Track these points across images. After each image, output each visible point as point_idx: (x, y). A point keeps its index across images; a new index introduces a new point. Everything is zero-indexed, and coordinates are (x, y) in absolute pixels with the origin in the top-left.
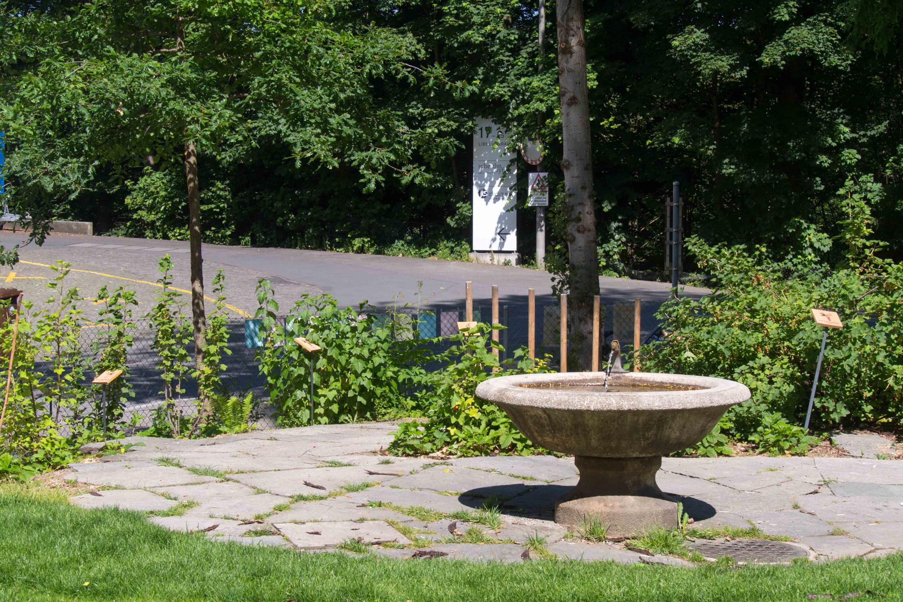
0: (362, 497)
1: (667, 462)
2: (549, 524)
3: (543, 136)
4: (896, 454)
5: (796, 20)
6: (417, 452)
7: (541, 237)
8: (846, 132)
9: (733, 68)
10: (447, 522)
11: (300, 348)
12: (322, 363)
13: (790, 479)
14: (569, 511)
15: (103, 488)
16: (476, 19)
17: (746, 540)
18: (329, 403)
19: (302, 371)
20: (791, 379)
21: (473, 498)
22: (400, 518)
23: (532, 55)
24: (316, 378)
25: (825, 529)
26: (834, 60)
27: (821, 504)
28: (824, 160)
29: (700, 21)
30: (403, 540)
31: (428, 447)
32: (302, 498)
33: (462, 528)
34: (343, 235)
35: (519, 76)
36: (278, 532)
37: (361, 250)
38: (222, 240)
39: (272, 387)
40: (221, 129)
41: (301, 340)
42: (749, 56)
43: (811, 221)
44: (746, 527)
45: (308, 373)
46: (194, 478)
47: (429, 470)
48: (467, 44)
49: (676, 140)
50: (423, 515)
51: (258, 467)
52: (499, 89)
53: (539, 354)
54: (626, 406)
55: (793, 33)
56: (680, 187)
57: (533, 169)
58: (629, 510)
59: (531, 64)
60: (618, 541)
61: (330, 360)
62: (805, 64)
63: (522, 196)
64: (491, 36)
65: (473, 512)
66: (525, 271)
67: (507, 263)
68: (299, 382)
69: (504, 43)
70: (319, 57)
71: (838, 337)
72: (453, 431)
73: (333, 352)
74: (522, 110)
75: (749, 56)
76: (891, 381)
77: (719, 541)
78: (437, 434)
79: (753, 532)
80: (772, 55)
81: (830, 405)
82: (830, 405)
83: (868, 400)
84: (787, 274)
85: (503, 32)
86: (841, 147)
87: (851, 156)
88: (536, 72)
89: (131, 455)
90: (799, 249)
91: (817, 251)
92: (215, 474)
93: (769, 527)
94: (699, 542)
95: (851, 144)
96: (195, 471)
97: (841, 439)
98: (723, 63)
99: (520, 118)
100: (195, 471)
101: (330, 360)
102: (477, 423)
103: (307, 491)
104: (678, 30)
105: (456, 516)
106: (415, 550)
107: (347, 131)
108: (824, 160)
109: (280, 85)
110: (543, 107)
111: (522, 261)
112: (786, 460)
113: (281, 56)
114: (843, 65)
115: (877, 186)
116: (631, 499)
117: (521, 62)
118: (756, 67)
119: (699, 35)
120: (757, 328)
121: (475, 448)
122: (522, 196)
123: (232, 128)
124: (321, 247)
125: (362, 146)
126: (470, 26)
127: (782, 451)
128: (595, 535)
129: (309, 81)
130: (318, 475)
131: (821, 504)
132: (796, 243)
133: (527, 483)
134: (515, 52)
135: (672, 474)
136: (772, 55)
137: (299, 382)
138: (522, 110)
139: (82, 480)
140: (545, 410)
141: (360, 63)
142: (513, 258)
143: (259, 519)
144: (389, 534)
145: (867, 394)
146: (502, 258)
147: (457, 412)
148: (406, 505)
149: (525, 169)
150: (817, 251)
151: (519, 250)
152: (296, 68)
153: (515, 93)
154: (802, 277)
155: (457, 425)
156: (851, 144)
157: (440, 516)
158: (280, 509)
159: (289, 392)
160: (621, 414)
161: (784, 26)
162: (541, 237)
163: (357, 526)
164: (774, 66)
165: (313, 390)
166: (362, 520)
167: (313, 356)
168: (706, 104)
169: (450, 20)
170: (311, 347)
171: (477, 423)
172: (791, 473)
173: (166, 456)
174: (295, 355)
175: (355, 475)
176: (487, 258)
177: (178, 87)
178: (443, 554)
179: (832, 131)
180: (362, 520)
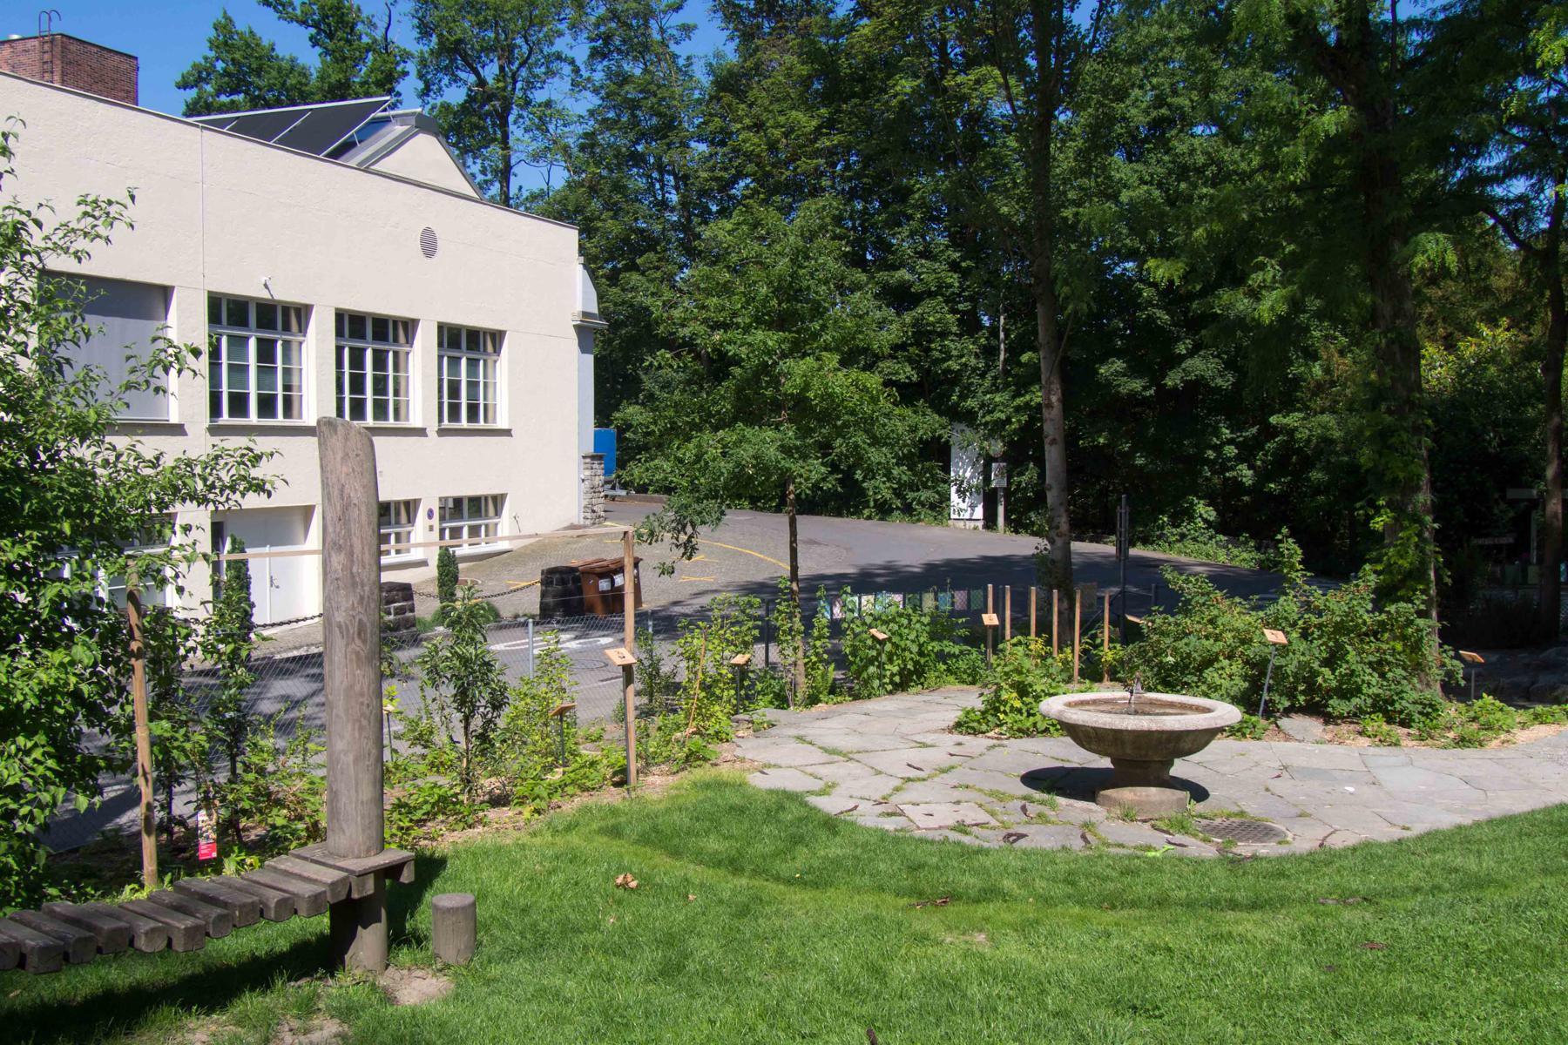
0: (951, 778)
1: (1177, 761)
2: (1092, 805)
3: (1003, 438)
4: (1328, 737)
5: (1191, 354)
6: (976, 732)
7: (1001, 509)
8: (1226, 433)
9: (1145, 388)
10: (1020, 803)
11: (873, 637)
12: (888, 647)
13: (1257, 764)
14: (1108, 798)
15: (769, 766)
16: (955, 353)
17: (1237, 820)
18: (893, 675)
19: (874, 653)
20: (1245, 678)
21: (1033, 779)
22: (983, 799)
23: (995, 378)
24: (884, 658)
25: (1294, 811)
26: (1219, 381)
27: (1283, 786)
28: (1211, 454)
29: (1119, 354)
30: (994, 823)
31: (984, 727)
32: (909, 780)
33: (1033, 809)
34: (856, 507)
35: (985, 393)
36: (902, 814)
37: (869, 518)
38: (769, 509)
39: (852, 663)
40: (818, 482)
41: (873, 631)
42: (1156, 379)
43: (1199, 498)
44: (1236, 809)
45: (879, 654)
46: (826, 757)
47: (992, 752)
48: (948, 371)
49: (1101, 440)
50: (1001, 797)
51: (869, 746)
52: (970, 403)
53: (1038, 634)
54: (1154, 727)
55: (1188, 363)
56: (1127, 499)
57: (996, 460)
58: (1153, 799)
59: (994, 384)
60: (1145, 821)
61: (894, 644)
62: (1196, 386)
63: (987, 480)
64: (965, 365)
65: (1037, 795)
66: (989, 534)
67: (976, 528)
68: (871, 661)
69: (974, 369)
70: (884, 425)
71: (1283, 650)
72: (1002, 716)
73: (895, 639)
74: (988, 418)
75: (1156, 379)
76: (1320, 680)
77: (1218, 821)
78: (990, 718)
79: (1242, 813)
80: (1173, 379)
81: (1276, 698)
82: (1276, 698)
83: (1302, 693)
84: (1183, 536)
85: (973, 361)
86: (1223, 444)
87: (1231, 451)
88: (997, 390)
89: (773, 731)
90: (1191, 519)
91: (1205, 521)
92: (840, 753)
93: (1253, 808)
94: (1204, 822)
95: (1231, 442)
96: (825, 750)
97: (1284, 722)
98: (1136, 385)
99: (986, 424)
100: (825, 750)
101: (894, 644)
102: (1019, 711)
103: (913, 773)
104: (1103, 360)
105: (1025, 798)
106: (1005, 832)
107: (905, 478)
108: (1211, 454)
109: (857, 446)
110: (1003, 416)
111: (986, 527)
112: (1248, 744)
113: (856, 424)
114: (1225, 385)
115: (1250, 473)
116: (1153, 790)
117: (987, 383)
118: (1161, 388)
119: (1119, 365)
120: (1217, 638)
121: (1019, 730)
122: (987, 480)
123: (824, 480)
124: (840, 515)
125: (913, 487)
126: (949, 358)
127: (1244, 735)
128: (1127, 817)
129: (876, 442)
130: (916, 756)
131: (1283, 786)
132: (1189, 514)
133: (1067, 765)
134: (983, 376)
135: (1179, 768)
136: (1173, 379)
137: (871, 661)
138: (988, 418)
139: (749, 756)
140: (1094, 728)
141: (913, 429)
142: (980, 524)
143: (885, 800)
144: (982, 817)
145: (1301, 688)
146: (971, 525)
147: (1005, 703)
148: (987, 787)
149: (989, 460)
150: (1205, 521)
151: (985, 518)
152: (866, 432)
153: (982, 406)
154: (1195, 539)
155: (1005, 712)
156: (1231, 442)
157: (1013, 797)
158: (897, 789)
159: (866, 668)
160: (1150, 733)
161: (1182, 358)
162: (1001, 509)
163: (956, 807)
164: (1175, 388)
165: (881, 666)
166: (958, 802)
167: (882, 643)
168: (1122, 410)
169: (936, 354)
170: (881, 636)
171: (1019, 711)
172: (1257, 758)
173: (802, 733)
174: (869, 642)
175: (937, 757)
176: (961, 524)
177: (786, 450)
178: (1023, 836)
179: (1216, 432)
180: (958, 802)
